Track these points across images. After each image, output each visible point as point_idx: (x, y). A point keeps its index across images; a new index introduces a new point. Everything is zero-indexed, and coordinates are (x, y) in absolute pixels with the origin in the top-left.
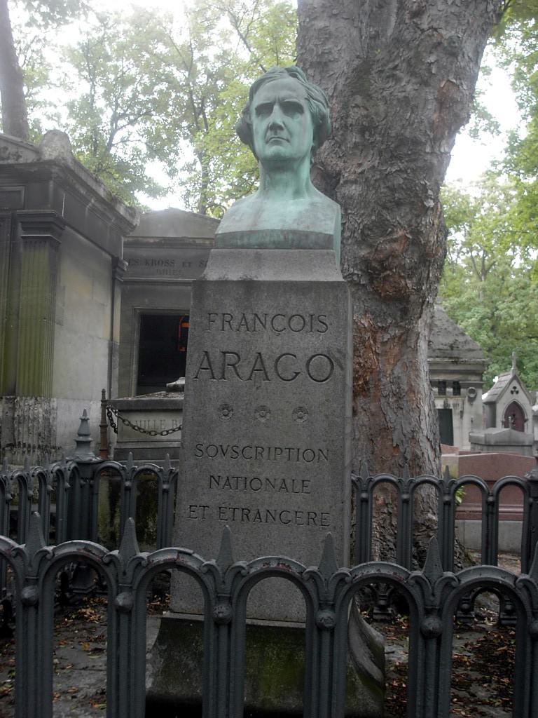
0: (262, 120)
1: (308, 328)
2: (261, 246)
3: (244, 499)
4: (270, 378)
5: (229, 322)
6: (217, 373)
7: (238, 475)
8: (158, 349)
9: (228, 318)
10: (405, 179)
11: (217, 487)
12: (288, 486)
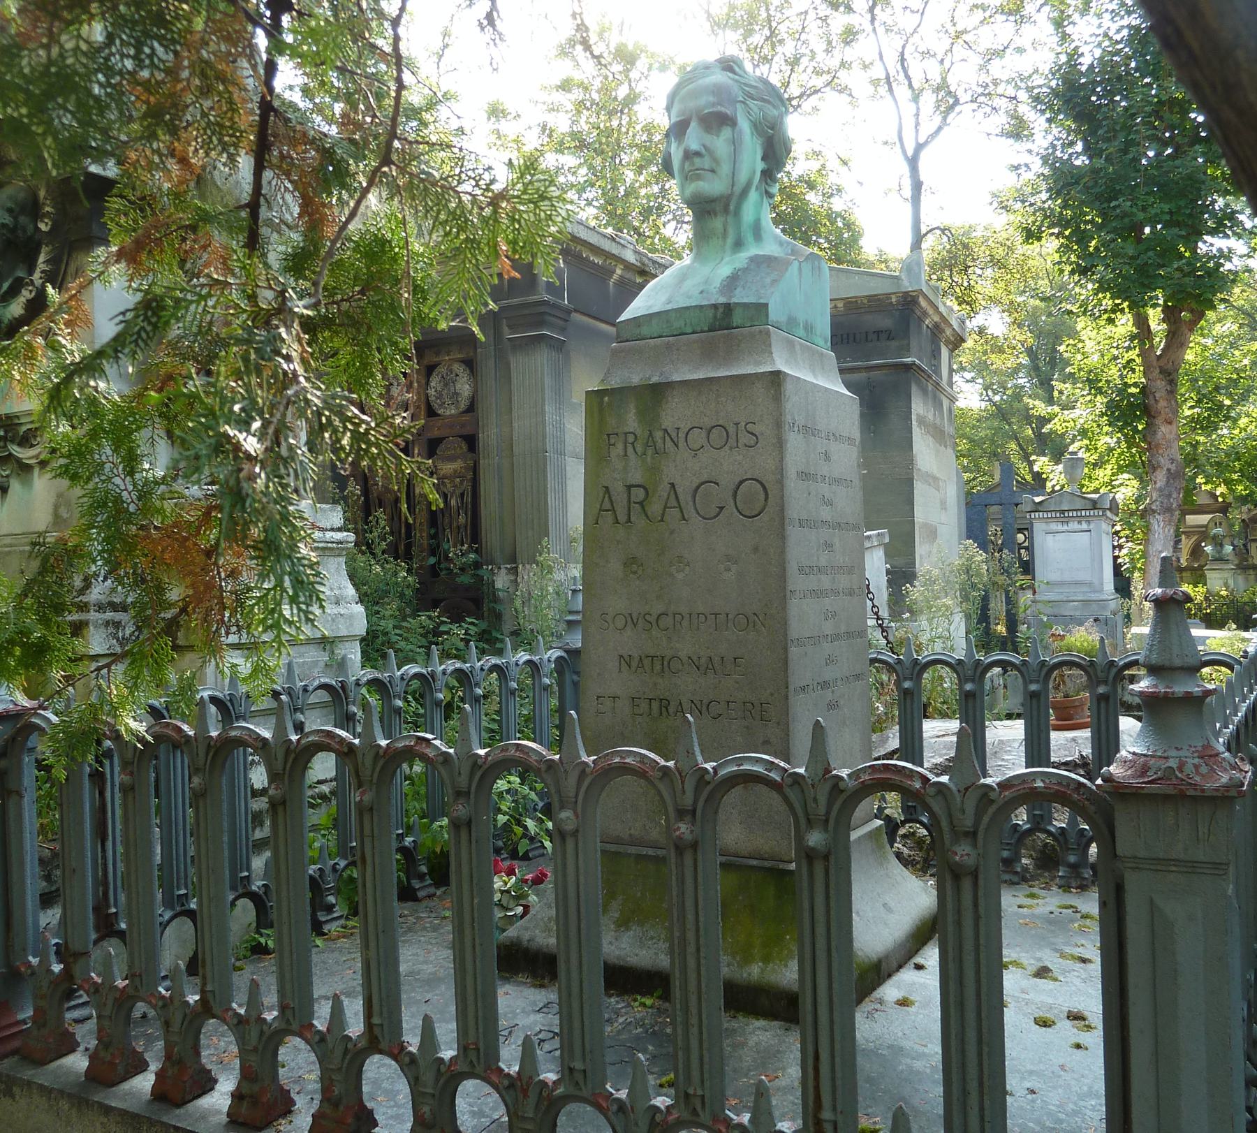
1: (732, 441)
6: (622, 517)
7: (652, 653)
9: (631, 438)
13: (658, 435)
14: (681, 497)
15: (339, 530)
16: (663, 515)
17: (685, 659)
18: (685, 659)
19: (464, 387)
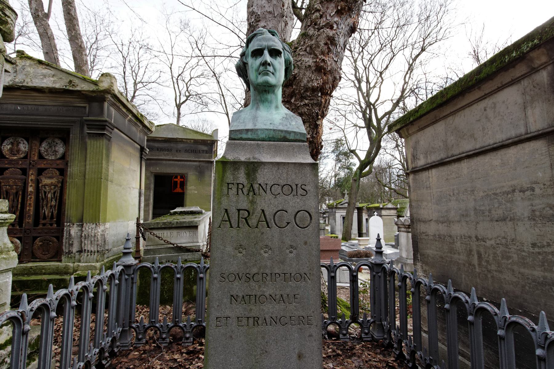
0: (255, 60)
1: (294, 192)
2: (437, 120)
3: (255, 311)
4: (270, 226)
5: (242, 189)
6: (235, 224)
7: (250, 294)
8: (166, 194)
10: (308, 109)
12: (284, 299)
13: (256, 186)
14: (267, 217)
15: (6, 213)
16: (257, 225)
17: (268, 296)
18: (268, 296)
19: (61, 149)
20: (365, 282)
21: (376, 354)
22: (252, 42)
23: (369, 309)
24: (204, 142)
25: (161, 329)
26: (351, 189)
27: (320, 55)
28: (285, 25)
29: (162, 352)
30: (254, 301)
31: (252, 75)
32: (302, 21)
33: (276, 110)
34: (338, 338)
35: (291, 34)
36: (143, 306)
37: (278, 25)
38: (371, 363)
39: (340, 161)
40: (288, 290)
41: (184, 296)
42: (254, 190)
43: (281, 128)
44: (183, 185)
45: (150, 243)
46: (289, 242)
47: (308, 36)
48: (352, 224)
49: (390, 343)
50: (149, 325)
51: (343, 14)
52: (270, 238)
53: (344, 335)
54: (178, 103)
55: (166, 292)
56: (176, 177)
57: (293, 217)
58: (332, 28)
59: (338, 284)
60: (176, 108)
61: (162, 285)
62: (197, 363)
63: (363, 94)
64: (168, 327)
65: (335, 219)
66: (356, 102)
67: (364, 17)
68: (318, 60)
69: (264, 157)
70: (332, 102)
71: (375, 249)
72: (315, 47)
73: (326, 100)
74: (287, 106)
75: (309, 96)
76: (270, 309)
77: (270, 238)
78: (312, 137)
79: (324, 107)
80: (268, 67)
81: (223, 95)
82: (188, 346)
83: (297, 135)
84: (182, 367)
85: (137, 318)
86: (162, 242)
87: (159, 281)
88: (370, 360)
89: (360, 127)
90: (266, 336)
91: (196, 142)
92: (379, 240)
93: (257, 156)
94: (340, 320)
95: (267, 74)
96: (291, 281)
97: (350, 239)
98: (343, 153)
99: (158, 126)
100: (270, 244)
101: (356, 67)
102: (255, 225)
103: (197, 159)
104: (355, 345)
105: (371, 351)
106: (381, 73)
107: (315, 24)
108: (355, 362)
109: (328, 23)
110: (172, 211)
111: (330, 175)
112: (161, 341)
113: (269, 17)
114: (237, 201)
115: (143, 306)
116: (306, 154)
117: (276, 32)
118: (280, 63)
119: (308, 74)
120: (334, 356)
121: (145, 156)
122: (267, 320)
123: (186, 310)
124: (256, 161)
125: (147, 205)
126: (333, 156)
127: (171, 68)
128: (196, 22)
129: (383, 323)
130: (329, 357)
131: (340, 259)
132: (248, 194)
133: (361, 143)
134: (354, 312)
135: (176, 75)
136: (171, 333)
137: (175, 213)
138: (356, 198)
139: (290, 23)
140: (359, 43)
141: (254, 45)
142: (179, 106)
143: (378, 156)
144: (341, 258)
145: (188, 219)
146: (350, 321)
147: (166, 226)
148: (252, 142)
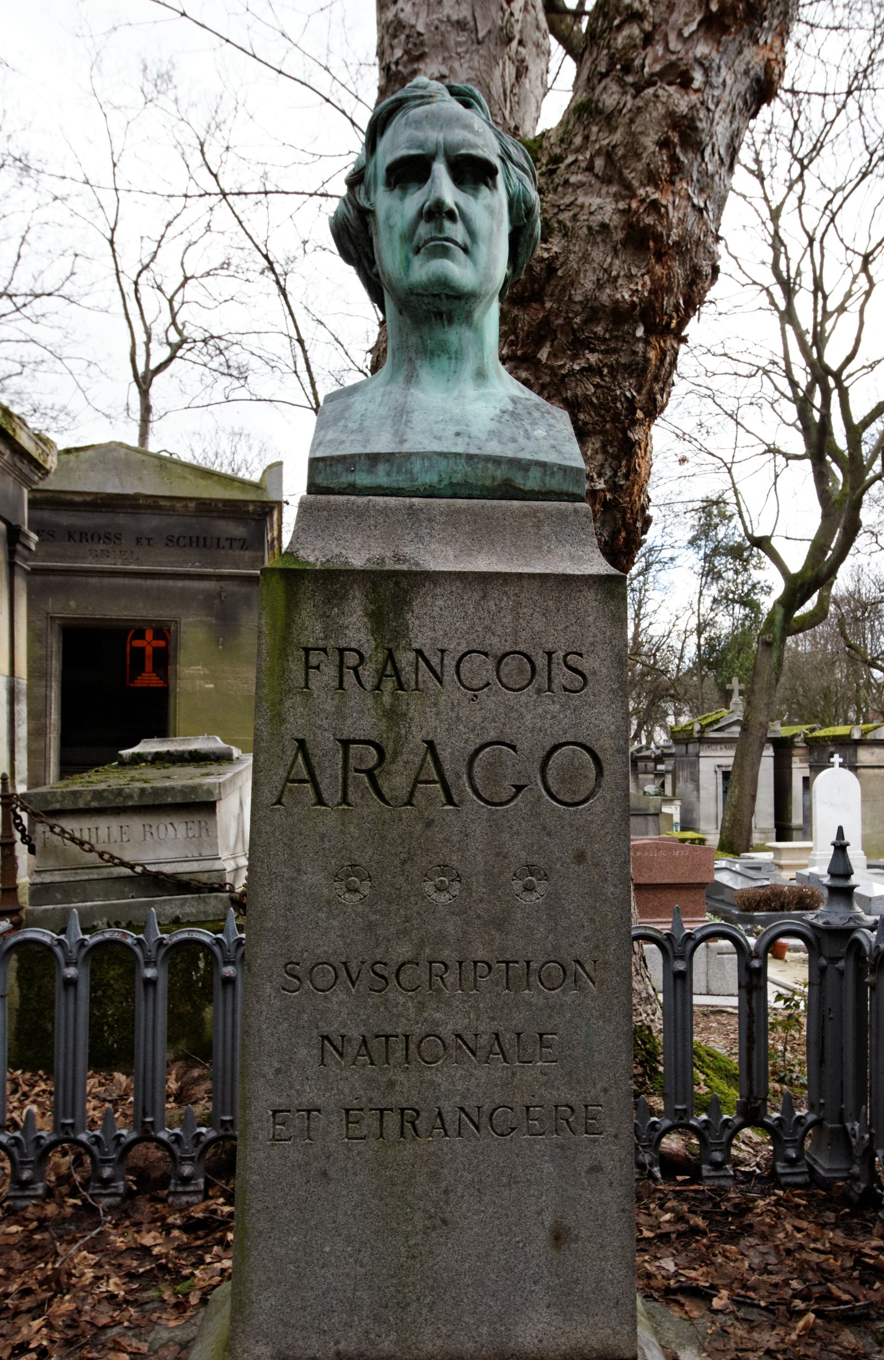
0: (402, 198)
1: (541, 680)
3: (407, 1087)
4: (456, 799)
5: (355, 669)
6: (331, 794)
7: (389, 1030)
9: (351, 659)
10: (597, 386)
11: (338, 1063)
13: (405, 658)
14: (447, 766)
16: (412, 794)
17: (450, 1039)
18: (450, 1039)
20: (794, 992)
21: (823, 1226)
22: (389, 132)
23: (804, 1080)
24: (232, 510)
25: (95, 1149)
26: (752, 675)
27: (643, 185)
28: (519, 76)
29: (99, 1223)
30: (400, 1054)
31: (390, 255)
32: (578, 58)
33: (478, 386)
34: (696, 1177)
35: (538, 108)
36: (35, 1074)
37: (490, 72)
38: (804, 1255)
39: (719, 576)
40: (519, 1018)
41: (172, 1040)
42: (397, 673)
43: (494, 448)
44: (164, 660)
45: (51, 864)
46: (523, 854)
47: (600, 112)
48: (754, 797)
49: (869, 1190)
50: (54, 1138)
51: (725, 30)
52: (455, 838)
53: (717, 1166)
54: (141, 369)
55: (111, 1027)
56: (140, 634)
57: (537, 765)
58: (685, 83)
59: (697, 1000)
60: (135, 388)
61: (95, 1002)
62: (219, 1259)
63: (800, 336)
64: (119, 1144)
65: (695, 779)
66: (774, 363)
67: (811, 47)
68: (634, 205)
69: (432, 552)
70: (686, 361)
71: (826, 880)
72: (624, 157)
73: (663, 353)
74: (524, 375)
75: (600, 327)
76: (457, 1083)
77: (455, 838)
78: (614, 487)
79: (656, 379)
80: (447, 224)
81: (301, 341)
82: (189, 1204)
83: (553, 474)
84: (169, 1272)
85: (15, 1115)
86: (93, 857)
87: (84, 989)
88: (801, 1247)
89: (788, 457)
90: (446, 1171)
91: (205, 507)
92: (840, 848)
93: (408, 550)
94: (704, 1117)
95: (445, 253)
96: (528, 986)
97: (748, 848)
98: (728, 549)
99: (68, 451)
100: (454, 860)
101: (776, 236)
102: (404, 793)
103: (210, 570)
104: (754, 1200)
105: (805, 1219)
106: (867, 259)
107: (627, 69)
108: (751, 1253)
109: (672, 65)
110: (126, 752)
111: (681, 625)
112: (95, 1188)
113: (459, 44)
114: (340, 712)
115: (35, 1074)
116: (582, 543)
117: (477, 92)
118: (491, 211)
119: (598, 254)
120: (680, 1235)
121: (26, 560)
122: (448, 1118)
123: (181, 1089)
124: (405, 567)
125: (37, 733)
126: (693, 560)
127: (112, 242)
128: (202, 69)
129: (849, 1125)
130: (664, 1238)
131: (708, 916)
132: (378, 688)
133: (791, 514)
134: (751, 1091)
135: (130, 270)
136: (130, 1162)
137: (138, 759)
138: (768, 705)
139: (535, 69)
140: (791, 149)
141: (396, 145)
142: (144, 382)
143: (849, 560)
144: (715, 913)
145: (182, 778)
146: (738, 1121)
147: (104, 804)
148: (392, 501)
